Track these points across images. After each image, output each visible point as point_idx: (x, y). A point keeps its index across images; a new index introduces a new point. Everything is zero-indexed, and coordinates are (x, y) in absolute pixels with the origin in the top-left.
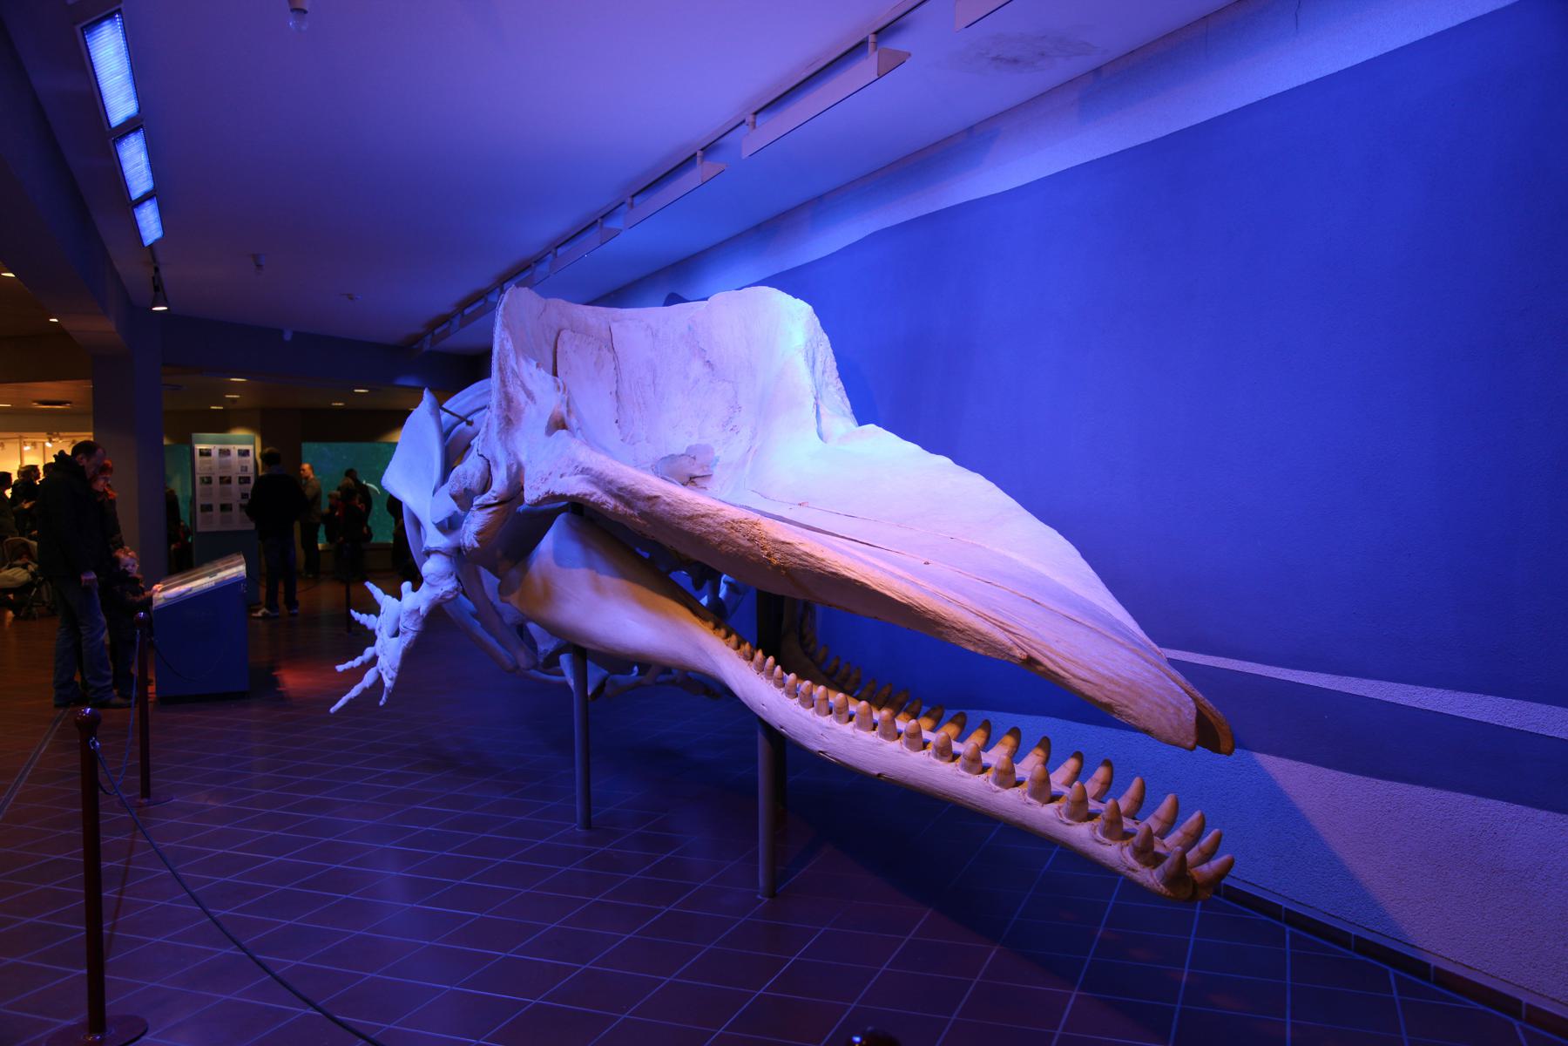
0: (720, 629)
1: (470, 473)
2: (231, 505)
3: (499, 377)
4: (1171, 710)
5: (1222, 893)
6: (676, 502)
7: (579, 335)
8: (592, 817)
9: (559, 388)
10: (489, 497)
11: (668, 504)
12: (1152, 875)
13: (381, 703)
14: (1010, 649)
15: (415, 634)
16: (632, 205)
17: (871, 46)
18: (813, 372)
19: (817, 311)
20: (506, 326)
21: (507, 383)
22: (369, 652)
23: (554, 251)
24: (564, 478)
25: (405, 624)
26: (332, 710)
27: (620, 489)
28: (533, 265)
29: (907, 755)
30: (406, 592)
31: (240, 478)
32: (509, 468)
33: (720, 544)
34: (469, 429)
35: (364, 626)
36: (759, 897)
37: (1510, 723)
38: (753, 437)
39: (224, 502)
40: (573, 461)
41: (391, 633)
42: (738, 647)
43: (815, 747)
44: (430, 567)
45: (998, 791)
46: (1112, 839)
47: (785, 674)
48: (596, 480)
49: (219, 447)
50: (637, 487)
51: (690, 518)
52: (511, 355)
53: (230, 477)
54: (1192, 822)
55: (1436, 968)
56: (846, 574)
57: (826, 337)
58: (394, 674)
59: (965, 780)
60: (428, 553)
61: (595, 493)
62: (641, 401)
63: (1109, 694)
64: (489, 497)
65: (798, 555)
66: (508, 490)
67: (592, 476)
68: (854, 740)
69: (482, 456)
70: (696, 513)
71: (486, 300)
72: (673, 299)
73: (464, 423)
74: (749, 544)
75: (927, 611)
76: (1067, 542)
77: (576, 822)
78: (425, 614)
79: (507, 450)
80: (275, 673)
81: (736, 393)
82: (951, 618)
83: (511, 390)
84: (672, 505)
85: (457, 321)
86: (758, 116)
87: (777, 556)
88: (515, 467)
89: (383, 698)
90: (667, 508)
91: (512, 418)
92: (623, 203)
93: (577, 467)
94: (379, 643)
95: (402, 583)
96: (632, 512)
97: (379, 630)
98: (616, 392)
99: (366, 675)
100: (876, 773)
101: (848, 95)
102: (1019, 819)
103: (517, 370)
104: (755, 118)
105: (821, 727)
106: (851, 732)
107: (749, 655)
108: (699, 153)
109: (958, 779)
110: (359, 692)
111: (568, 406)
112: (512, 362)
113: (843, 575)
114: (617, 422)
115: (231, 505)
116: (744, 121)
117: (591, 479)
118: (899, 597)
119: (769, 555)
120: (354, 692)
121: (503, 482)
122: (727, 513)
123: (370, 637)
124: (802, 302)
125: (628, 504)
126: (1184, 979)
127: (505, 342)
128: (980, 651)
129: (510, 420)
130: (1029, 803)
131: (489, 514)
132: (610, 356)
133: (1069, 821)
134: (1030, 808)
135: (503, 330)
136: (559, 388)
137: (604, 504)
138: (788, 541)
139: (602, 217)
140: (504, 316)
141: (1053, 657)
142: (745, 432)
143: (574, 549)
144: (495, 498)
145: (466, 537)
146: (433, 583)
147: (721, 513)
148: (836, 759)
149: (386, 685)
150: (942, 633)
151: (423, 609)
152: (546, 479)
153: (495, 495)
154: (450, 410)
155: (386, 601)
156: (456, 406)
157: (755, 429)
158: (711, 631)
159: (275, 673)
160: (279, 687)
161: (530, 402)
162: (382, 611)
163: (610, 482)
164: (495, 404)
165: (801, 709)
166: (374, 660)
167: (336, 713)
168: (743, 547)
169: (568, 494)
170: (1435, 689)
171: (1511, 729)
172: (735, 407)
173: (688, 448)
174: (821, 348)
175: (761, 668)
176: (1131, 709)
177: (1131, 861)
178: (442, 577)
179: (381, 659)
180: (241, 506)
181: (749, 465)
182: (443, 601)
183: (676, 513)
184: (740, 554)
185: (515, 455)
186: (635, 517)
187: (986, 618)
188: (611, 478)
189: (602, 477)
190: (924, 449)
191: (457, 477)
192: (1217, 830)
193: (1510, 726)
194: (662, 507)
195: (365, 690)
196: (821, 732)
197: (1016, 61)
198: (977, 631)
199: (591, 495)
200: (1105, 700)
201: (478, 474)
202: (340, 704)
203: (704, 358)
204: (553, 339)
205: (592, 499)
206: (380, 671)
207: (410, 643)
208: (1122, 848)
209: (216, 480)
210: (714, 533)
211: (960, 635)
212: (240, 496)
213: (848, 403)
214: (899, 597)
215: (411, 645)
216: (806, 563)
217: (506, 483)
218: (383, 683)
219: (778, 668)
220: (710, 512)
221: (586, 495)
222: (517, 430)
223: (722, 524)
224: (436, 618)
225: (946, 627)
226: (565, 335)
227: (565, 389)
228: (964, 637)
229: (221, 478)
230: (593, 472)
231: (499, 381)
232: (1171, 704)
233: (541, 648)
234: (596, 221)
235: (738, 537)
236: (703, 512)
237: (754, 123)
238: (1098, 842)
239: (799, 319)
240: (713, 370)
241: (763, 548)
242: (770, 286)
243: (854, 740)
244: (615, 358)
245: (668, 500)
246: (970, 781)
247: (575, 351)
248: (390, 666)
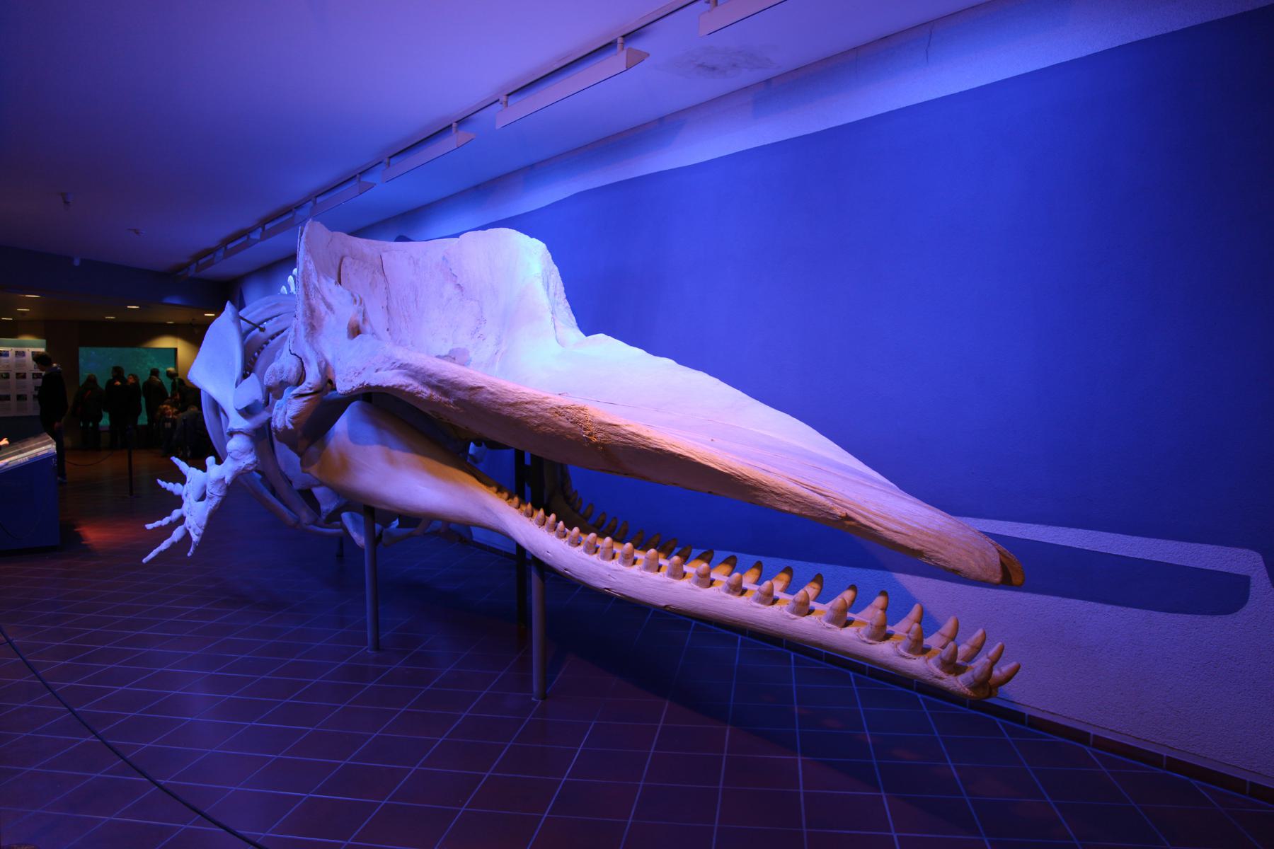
0: (502, 493)
1: (287, 367)
2: (26, 395)
3: (303, 292)
4: (977, 554)
5: (867, 673)
6: (500, 392)
7: (357, 261)
8: (380, 638)
9: (356, 301)
10: (303, 388)
11: (492, 393)
12: (958, 681)
13: (189, 554)
14: (831, 509)
15: (220, 499)
16: (389, 165)
17: (619, 46)
18: (548, 294)
19: (550, 249)
20: (309, 251)
21: (310, 297)
22: (176, 513)
23: (314, 199)
24: (378, 373)
25: (212, 491)
26: (144, 561)
27: (441, 381)
28: (294, 210)
29: (699, 591)
30: (210, 465)
31: (34, 374)
32: (319, 365)
33: (538, 426)
34: (262, 334)
35: (171, 493)
36: (533, 699)
37: (1087, 546)
38: (499, 343)
39: (20, 393)
40: (390, 358)
41: (197, 498)
42: (518, 507)
43: (602, 585)
44: (234, 444)
45: (795, 619)
46: (915, 654)
47: (567, 530)
48: (414, 374)
49: (15, 349)
50: (461, 379)
51: (513, 405)
52: (313, 274)
53: (25, 374)
54: (977, 638)
55: (1029, 716)
56: (671, 449)
57: (556, 268)
58: (201, 531)
59: (759, 610)
60: (232, 434)
61: (411, 385)
62: (406, 313)
63: (920, 542)
64: (303, 388)
65: (623, 435)
66: (321, 382)
67: (410, 370)
68: (641, 579)
69: (295, 355)
70: (520, 400)
71: (249, 237)
72: (402, 239)
73: (257, 330)
74: (572, 426)
75: (748, 479)
76: (802, 423)
77: (367, 645)
78: (229, 483)
79: (314, 349)
80: (76, 530)
81: (481, 309)
82: (773, 484)
83: (313, 302)
84: (496, 394)
85: (220, 254)
86: (509, 97)
87: (599, 435)
88: (324, 364)
89: (191, 550)
90: (490, 397)
91: (315, 324)
92: (380, 163)
93: (394, 363)
94: (186, 506)
95: (207, 457)
96: (447, 400)
97: (186, 495)
98: (387, 307)
99: (174, 532)
100: (663, 604)
101: (587, 86)
102: (817, 640)
103: (318, 286)
104: (507, 99)
105: (608, 569)
106: (639, 574)
107: (530, 513)
108: (454, 125)
109: (754, 609)
110: (168, 546)
111: (364, 315)
112: (314, 280)
113: (668, 451)
114: (388, 330)
115: (26, 395)
116: (498, 100)
117: (410, 373)
118: (722, 468)
119: (589, 435)
120: (165, 545)
121: (317, 376)
122: (553, 400)
123: (178, 501)
124: (538, 241)
125: (446, 393)
126: (869, 740)
127: (308, 264)
128: (795, 510)
129: (314, 326)
130: (829, 628)
131: (305, 401)
132: (380, 278)
133: (870, 641)
134: (829, 632)
135: (307, 254)
136: (356, 301)
137: (418, 393)
138: (615, 423)
139: (360, 173)
140: (306, 243)
141: (866, 514)
142: (491, 340)
143: (367, 430)
144: (311, 389)
145: (278, 422)
146: (237, 458)
147: (547, 401)
148: (620, 594)
149: (194, 540)
150: (758, 496)
151: (228, 478)
152: (359, 373)
153: (310, 386)
154: (246, 318)
155: (192, 473)
156: (254, 313)
157: (499, 337)
158: (495, 495)
159: (76, 530)
160: (83, 541)
161: (329, 312)
162: (188, 480)
163: (430, 376)
164: (301, 313)
165: (586, 556)
166: (182, 520)
167: (147, 563)
168: (561, 427)
169: (385, 385)
170: (1032, 525)
171: (1088, 550)
172: (481, 320)
173: (450, 351)
174: (553, 276)
175: (542, 523)
176: (942, 554)
177: (937, 671)
178: (244, 453)
179: (188, 519)
180: (34, 396)
181: (497, 364)
182: (244, 472)
183: (498, 401)
184: (558, 434)
185: (322, 355)
186: (450, 403)
187: (796, 482)
188: (432, 372)
189: (423, 371)
190: (648, 352)
191: (274, 372)
192: (1000, 643)
193: (1087, 548)
194: (485, 395)
195: (174, 544)
196: (608, 573)
197: (714, 69)
198: (797, 495)
199: (407, 386)
200: (917, 547)
201: (294, 369)
202: (152, 555)
203: (455, 281)
204: (338, 264)
205: (407, 389)
206: (188, 529)
207: (216, 506)
208: (926, 661)
209: (13, 375)
210: (535, 417)
211: (777, 498)
212: (33, 388)
213: (574, 318)
214: (722, 468)
215: (217, 507)
216: (630, 441)
217: (319, 376)
218: (191, 538)
219: (561, 524)
220: (535, 400)
221: (401, 386)
222: (320, 335)
223: (546, 409)
224: (236, 488)
225: (766, 492)
226: (347, 261)
227: (361, 303)
229: (17, 374)
230: (413, 367)
231: (303, 295)
232: (977, 549)
233: (324, 507)
234: (355, 176)
235: (560, 420)
236: (528, 399)
237: (507, 102)
238: (904, 656)
239: (535, 254)
240: (462, 291)
241: (585, 429)
242: (510, 228)
243: (641, 579)
244: (386, 280)
245: (493, 390)
246: (765, 611)
247: (354, 274)
248: (197, 524)
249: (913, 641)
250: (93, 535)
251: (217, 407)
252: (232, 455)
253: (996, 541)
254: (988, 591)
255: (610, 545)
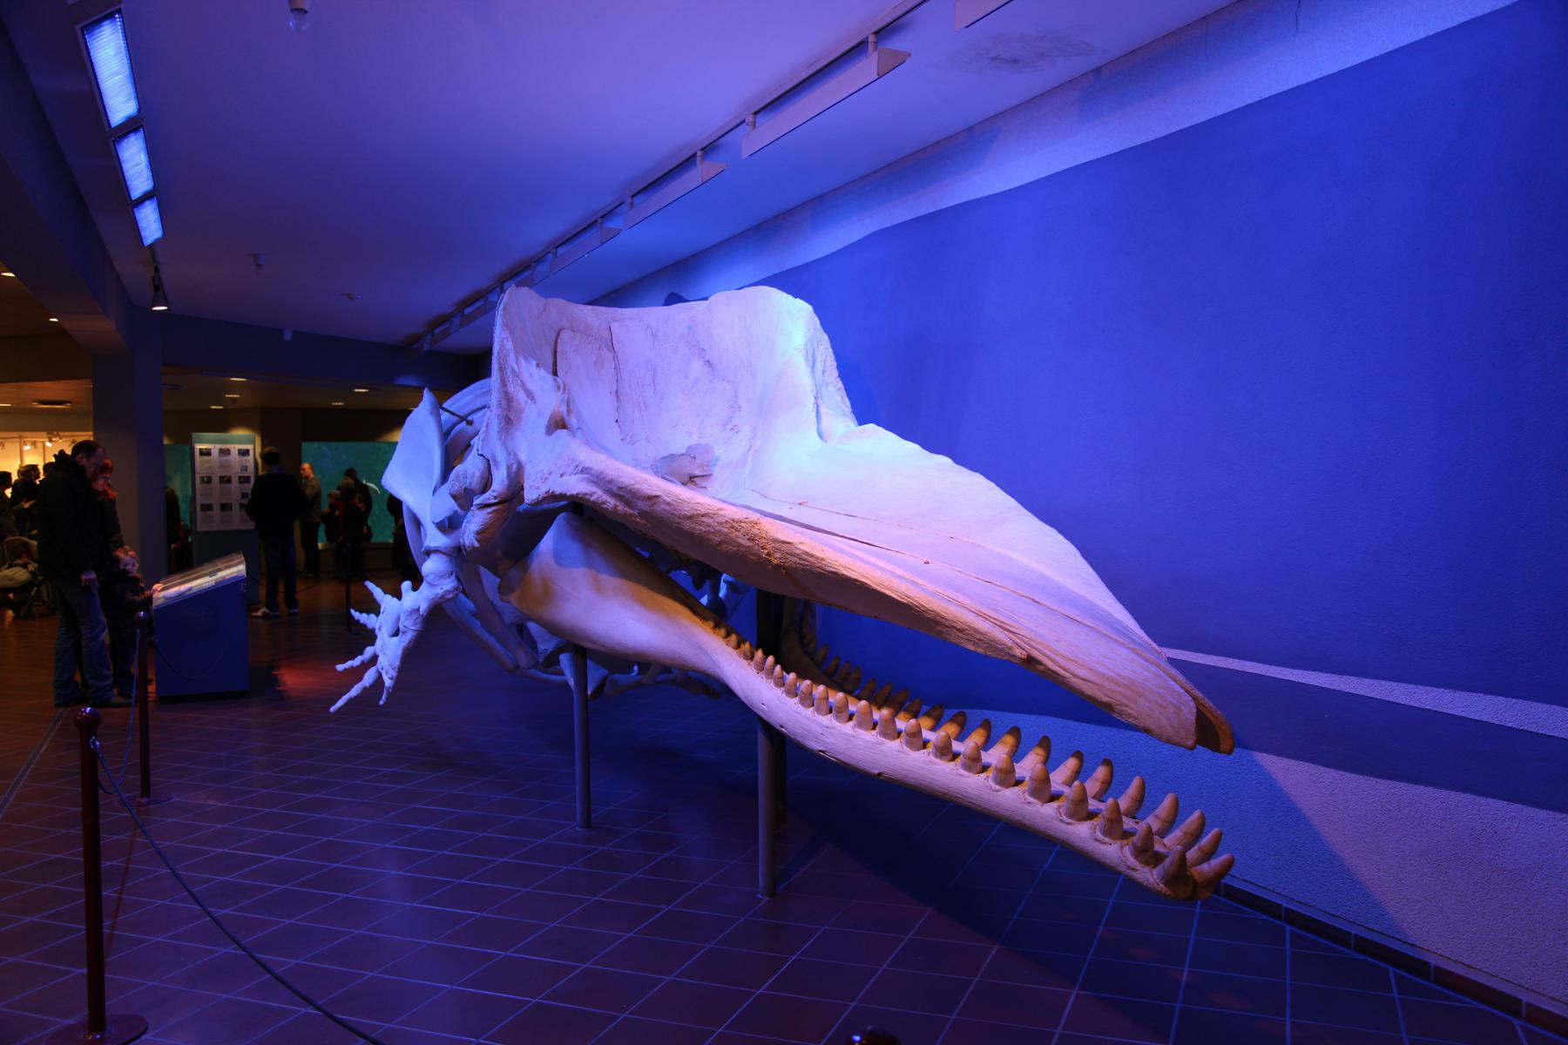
0: (720, 628)
1: (470, 472)
2: (231, 504)
3: (499, 377)
4: (1171, 709)
5: (1222, 892)
6: (676, 502)
7: (579, 335)
8: (592, 816)
9: (559, 387)
10: (489, 497)
11: (668, 504)
12: (1152, 874)
13: (381, 703)
14: (1010, 649)
15: (415, 634)
16: (632, 205)
17: (871, 46)
18: (813, 371)
19: (817, 311)
20: (506, 326)
21: (507, 383)
22: (369, 651)
23: (554, 251)
24: (564, 478)
25: (405, 624)
26: (332, 709)
27: (620, 488)
28: (533, 265)
29: (907, 754)
30: (406, 592)
31: (240, 477)
32: (509, 468)
33: (720, 543)
35: (364, 626)
36: (759, 896)
37: (1510, 722)
38: (753, 437)
39: (224, 502)
40: (573, 460)
41: (391, 633)
42: (738, 647)
43: (815, 746)
44: (430, 566)
45: (998, 791)
46: (1112, 838)
47: (785, 673)
48: (596, 479)
49: (219, 446)
50: (637, 486)
51: (690, 518)
52: (511, 355)
53: (230, 477)
54: (1192, 821)
55: (1436, 967)
56: (846, 573)
57: (826, 337)
58: (394, 674)
59: (965, 780)
60: (428, 553)
61: (595, 493)
62: (641, 400)
63: (1109, 693)
64: (489, 497)
65: (798, 555)
66: (508, 489)
67: (592, 475)
68: (854, 739)
69: (482, 455)
70: (696, 512)
71: (486, 300)
72: (673, 299)
73: (464, 423)
74: (749, 544)
75: (927, 611)
76: (1067, 542)
77: (576, 822)
78: (425, 614)
79: (507, 449)
80: (275, 673)
81: (736, 392)
82: (951, 617)
83: (511, 389)
84: (672, 505)
85: (457, 321)
86: (758, 115)
87: (777, 555)
88: (515, 467)
89: (383, 698)
90: (667, 508)
91: (512, 418)
92: (623, 203)
93: (577, 466)
94: (379, 642)
95: (402, 583)
96: (632, 511)
97: (379, 629)
98: (616, 392)
99: (366, 675)
100: (876, 772)
101: (848, 94)
102: (1019, 818)
103: (517, 370)
104: (755, 118)
105: (821, 726)
106: (851, 732)
107: (749, 654)
108: (699, 153)
109: (958, 778)
110: (359, 692)
111: (568, 405)
112: (512, 361)
113: (843, 575)
114: (617, 421)
115: (231, 504)
116: (744, 121)
117: (591, 478)
118: (899, 596)
119: (769, 554)
120: (354, 691)
121: (503, 481)
122: (727, 512)
123: (370, 637)
124: (802, 301)
125: (628, 503)
126: (1184, 978)
127: (505, 341)
128: (980, 651)
129: (510, 419)
130: (1029, 803)
131: (489, 513)
132: (610, 355)
133: (1069, 820)
134: (1030, 808)
135: (503, 330)
136: (559, 387)
137: (604, 503)
138: (788, 540)
139: (602, 217)
140: (504, 316)
141: (1053, 656)
142: (745, 432)
143: (574, 549)
144: (495, 498)
145: (466, 537)
146: (433, 583)
147: (721, 513)
148: (836, 758)
149: (386, 685)
150: (942, 632)
151: (423, 608)
152: (546, 479)
153: (495, 494)
154: (450, 409)
155: (386, 601)
156: (456, 405)
157: (755, 428)
158: (711, 631)
159: (275, 673)
160: (279, 686)
161: (530, 401)
162: (382, 610)
163: (610, 482)
164: (495, 404)
165: (801, 708)
166: (374, 660)
167: (336, 712)
168: (743, 546)
169: (568, 494)
170: (1435, 689)
171: (1511, 728)
172: (735, 407)
173: (688, 448)
174: (821, 348)
175: (761, 668)
176: (1131, 709)
177: (1131, 860)
178: (442, 577)
179: (381, 659)
180: (241, 506)
181: (749, 464)
182: (443, 600)
183: (676, 513)
184: (740, 553)
185: (515, 455)
186: (635, 516)
187: (986, 618)
188: (611, 478)
189: (602, 476)
190: (924, 449)
191: (457, 476)
192: (1217, 829)
193: (1510, 725)
194: (662, 506)
195: (365, 689)
196: (821, 731)
197: (1016, 61)
198: (977, 631)
199: (591, 495)
200: (1105, 699)
201: (478, 474)
202: (340, 703)
203: (704, 357)
204: (553, 339)
205: (592, 499)
206: (380, 670)
207: (410, 642)
208: (1122, 847)
209: (216, 480)
210: (714, 533)
211: (960, 635)
212: (240, 495)
213: (848, 403)
214: (899, 596)
215: (411, 645)
216: (806, 563)
217: (506, 483)
218: (383, 683)
219: (778, 668)
220: (710, 511)
221: (586, 494)
222: (517, 430)
223: (722, 524)
224: (436, 618)
225: (946, 626)
226: (565, 335)
227: (565, 389)
228: (964, 636)
229: (221, 478)
230: (593, 472)
231: (499, 381)
232: (1171, 703)
233: (541, 647)
234: (596, 221)
235: (738, 537)
236: (703, 511)
237: (754, 123)
238: (1098, 841)
239: (799, 319)
240: (713, 369)
241: (763, 548)
242: (770, 286)
243: (854, 739)
244: (615, 358)
245: (668, 500)
246: (970, 780)
247: (575, 351)
248: (390, 665)
249: (1108, 820)
250: (292, 680)
251: (417, 523)
252: (427, 579)
253: (1203, 694)
254: (1377, 782)
255: (823, 695)
